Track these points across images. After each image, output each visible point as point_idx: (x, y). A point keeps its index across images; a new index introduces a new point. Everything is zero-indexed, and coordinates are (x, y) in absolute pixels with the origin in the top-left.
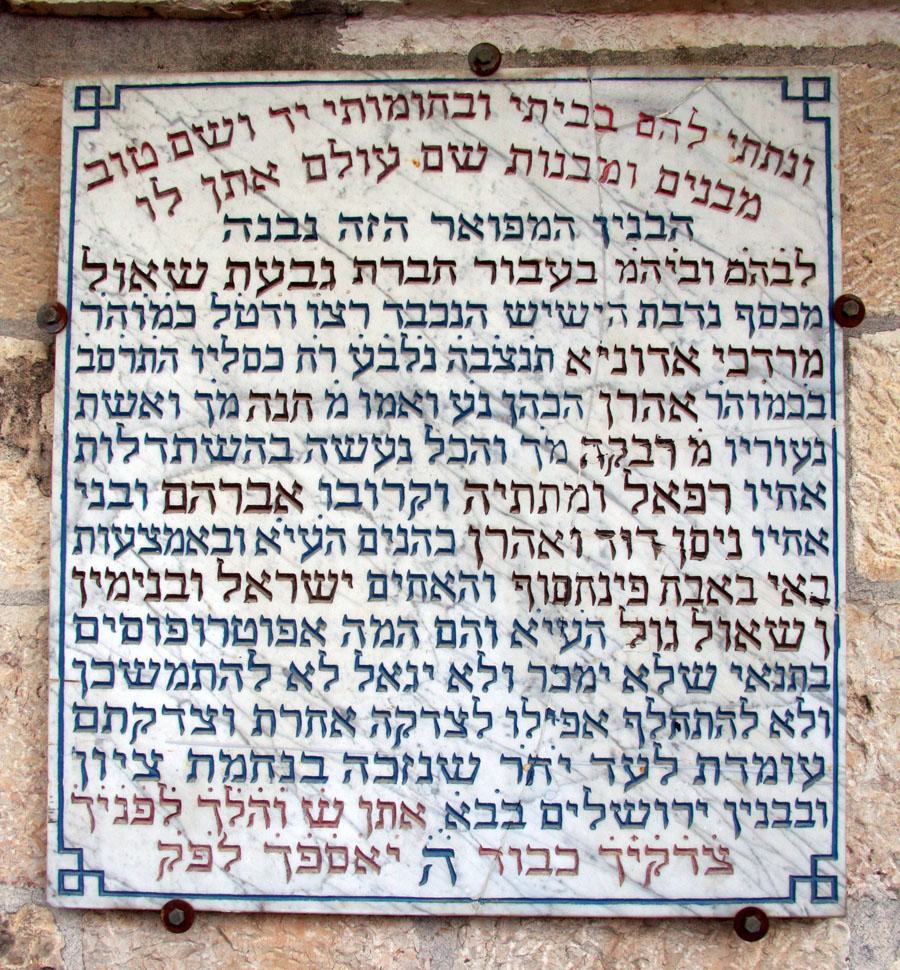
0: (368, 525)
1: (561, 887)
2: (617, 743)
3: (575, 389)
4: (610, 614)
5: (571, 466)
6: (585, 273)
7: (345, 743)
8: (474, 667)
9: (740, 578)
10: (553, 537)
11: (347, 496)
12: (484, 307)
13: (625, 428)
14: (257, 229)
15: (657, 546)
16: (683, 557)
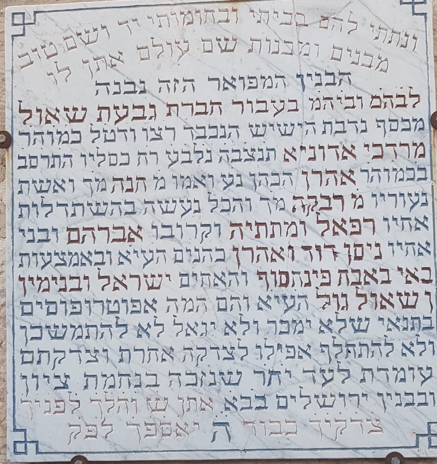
0: (178, 247)
1: (288, 442)
2: (317, 361)
3: (288, 170)
4: (310, 292)
5: (288, 212)
6: (293, 106)
7: (168, 366)
8: (238, 322)
9: (381, 270)
10: (279, 251)
11: (167, 232)
12: (237, 127)
13: (316, 190)
14: (113, 88)
15: (335, 253)
16: (350, 260)
